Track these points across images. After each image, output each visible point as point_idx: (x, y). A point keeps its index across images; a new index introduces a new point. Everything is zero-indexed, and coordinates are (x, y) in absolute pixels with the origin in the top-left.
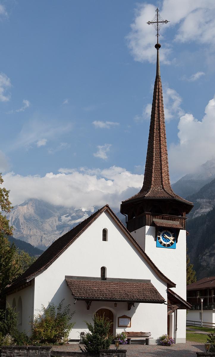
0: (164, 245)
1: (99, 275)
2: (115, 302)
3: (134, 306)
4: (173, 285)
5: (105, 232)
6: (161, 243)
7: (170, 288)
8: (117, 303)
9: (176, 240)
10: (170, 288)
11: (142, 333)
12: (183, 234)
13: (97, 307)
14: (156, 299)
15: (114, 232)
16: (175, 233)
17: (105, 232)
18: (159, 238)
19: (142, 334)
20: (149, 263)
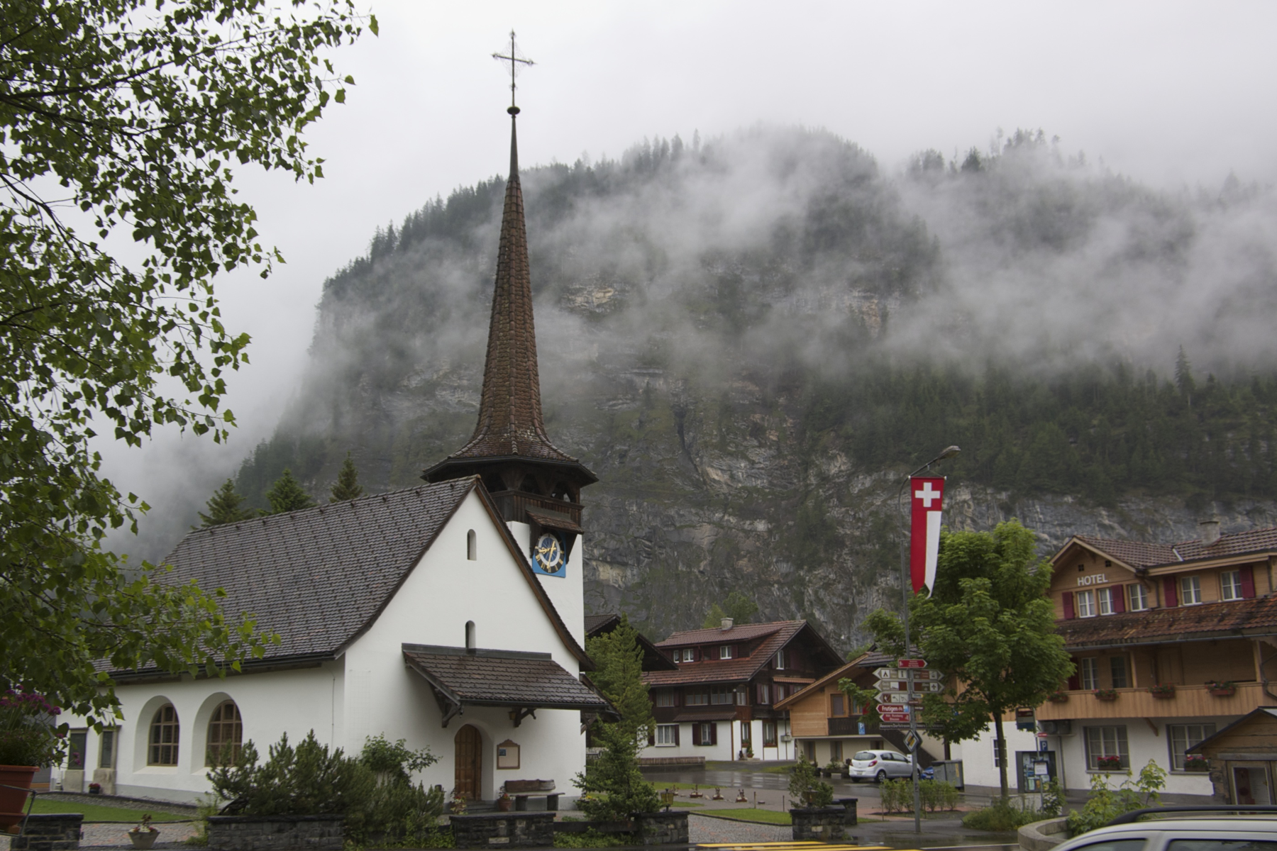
5: (471, 535)
17: (471, 535)
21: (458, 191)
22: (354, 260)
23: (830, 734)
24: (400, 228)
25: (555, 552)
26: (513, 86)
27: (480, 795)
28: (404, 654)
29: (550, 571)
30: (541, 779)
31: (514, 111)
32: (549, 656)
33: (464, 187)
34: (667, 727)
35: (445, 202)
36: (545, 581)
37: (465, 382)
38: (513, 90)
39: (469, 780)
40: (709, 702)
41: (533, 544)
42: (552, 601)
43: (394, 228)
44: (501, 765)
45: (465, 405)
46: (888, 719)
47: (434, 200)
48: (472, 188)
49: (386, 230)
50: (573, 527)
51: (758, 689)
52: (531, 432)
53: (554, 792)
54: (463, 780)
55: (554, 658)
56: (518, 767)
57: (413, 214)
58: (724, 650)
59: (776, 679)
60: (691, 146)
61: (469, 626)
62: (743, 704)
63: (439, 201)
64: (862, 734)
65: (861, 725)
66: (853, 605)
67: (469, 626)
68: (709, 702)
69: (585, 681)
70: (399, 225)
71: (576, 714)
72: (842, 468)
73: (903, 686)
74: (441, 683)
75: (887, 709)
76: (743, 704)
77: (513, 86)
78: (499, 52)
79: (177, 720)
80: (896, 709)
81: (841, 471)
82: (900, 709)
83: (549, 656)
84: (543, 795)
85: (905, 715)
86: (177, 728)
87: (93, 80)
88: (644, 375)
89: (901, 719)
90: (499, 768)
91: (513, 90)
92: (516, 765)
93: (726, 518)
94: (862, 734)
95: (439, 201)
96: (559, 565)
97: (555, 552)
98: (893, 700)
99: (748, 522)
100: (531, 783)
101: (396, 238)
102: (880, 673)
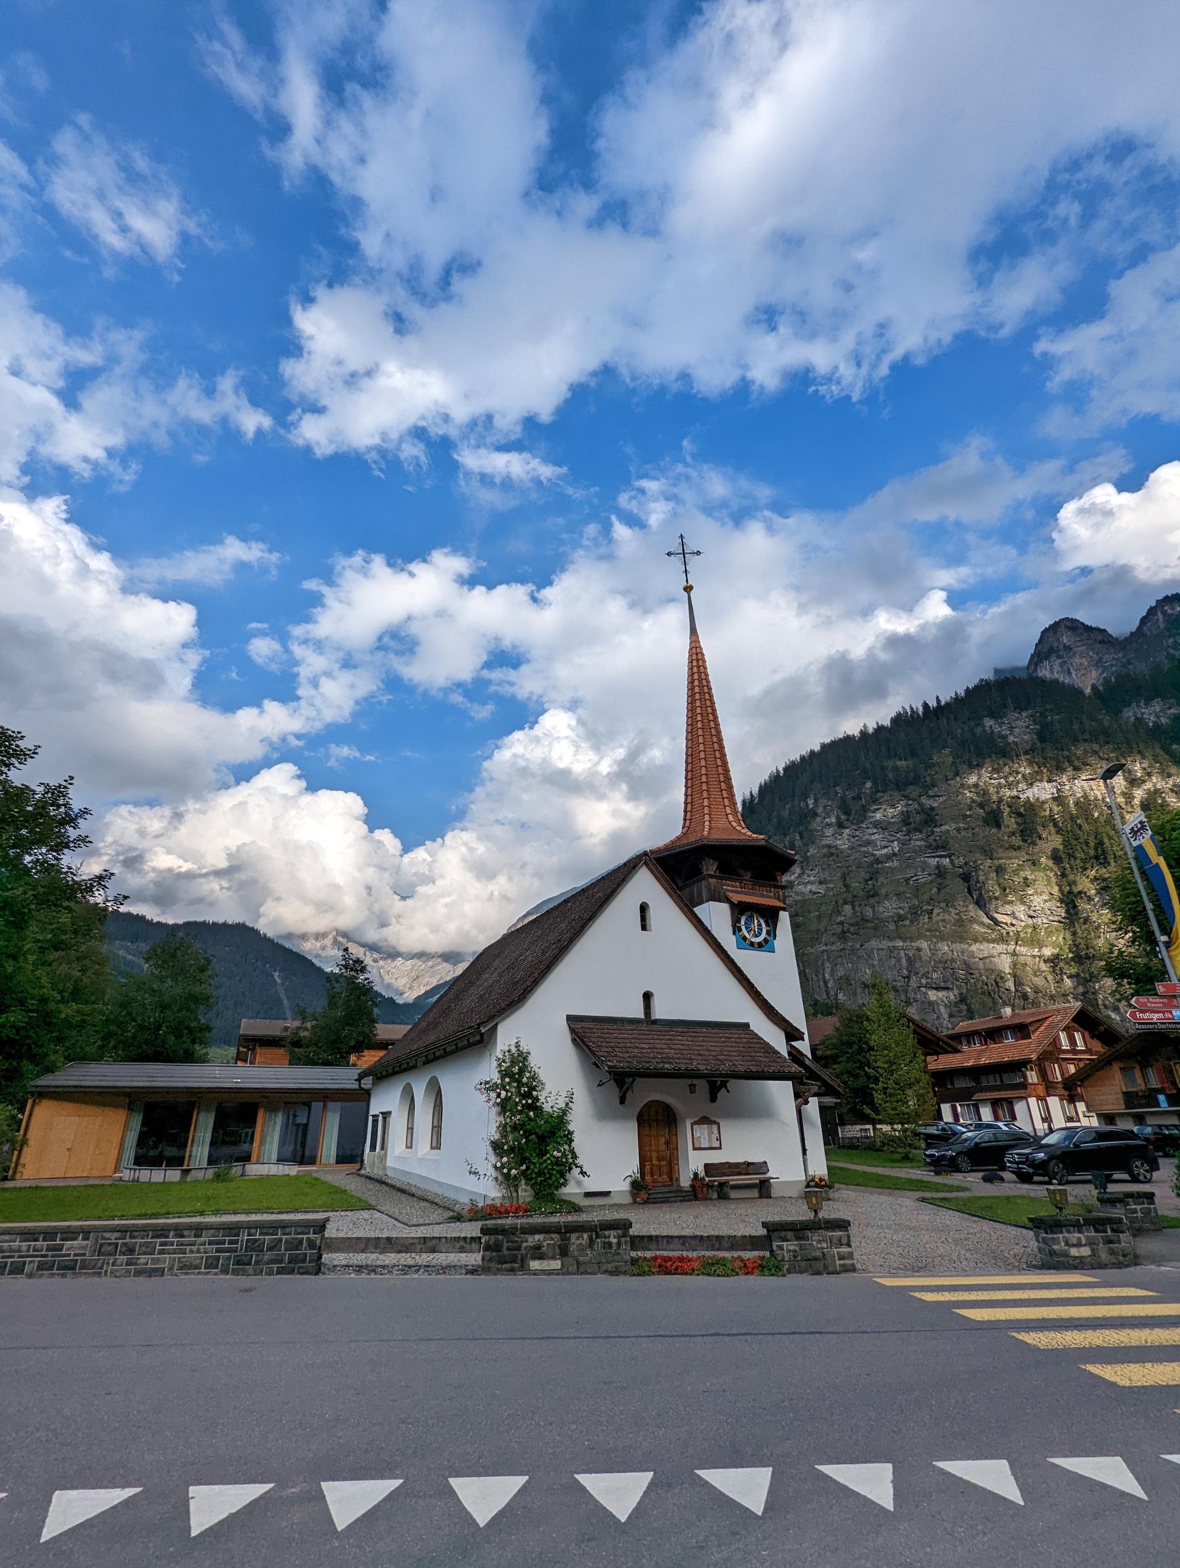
0: (752, 944)
1: (640, 1014)
2: (689, 1081)
3: (728, 1091)
4: (796, 1034)
5: (644, 908)
6: (745, 938)
7: (793, 1043)
8: (695, 1081)
9: (772, 933)
10: (793, 1043)
11: (749, 1164)
12: (784, 916)
13: (646, 1093)
14: (754, 1069)
15: (664, 908)
16: (771, 916)
17: (644, 908)
18: (740, 930)
19: (747, 1168)
20: (403, 1191)
25: (760, 925)
27: (678, 1180)
28: (572, 1031)
29: (756, 946)
32: (747, 1025)
34: (968, 1105)
37: (812, 878)
40: (1002, 1080)
42: (742, 969)
44: (697, 1145)
45: (815, 893)
51: (1048, 1069)
53: (769, 1175)
56: (720, 1148)
60: (935, 704)
61: (647, 996)
62: (1036, 1081)
63: (778, 771)
67: (647, 996)
68: (1002, 1080)
70: (756, 791)
78: (672, 550)
84: (755, 1179)
87: (315, 588)
88: (934, 857)
90: (695, 1149)
93: (1018, 948)
95: (778, 771)
96: (766, 941)
97: (760, 925)
99: (1037, 950)
100: (737, 1165)
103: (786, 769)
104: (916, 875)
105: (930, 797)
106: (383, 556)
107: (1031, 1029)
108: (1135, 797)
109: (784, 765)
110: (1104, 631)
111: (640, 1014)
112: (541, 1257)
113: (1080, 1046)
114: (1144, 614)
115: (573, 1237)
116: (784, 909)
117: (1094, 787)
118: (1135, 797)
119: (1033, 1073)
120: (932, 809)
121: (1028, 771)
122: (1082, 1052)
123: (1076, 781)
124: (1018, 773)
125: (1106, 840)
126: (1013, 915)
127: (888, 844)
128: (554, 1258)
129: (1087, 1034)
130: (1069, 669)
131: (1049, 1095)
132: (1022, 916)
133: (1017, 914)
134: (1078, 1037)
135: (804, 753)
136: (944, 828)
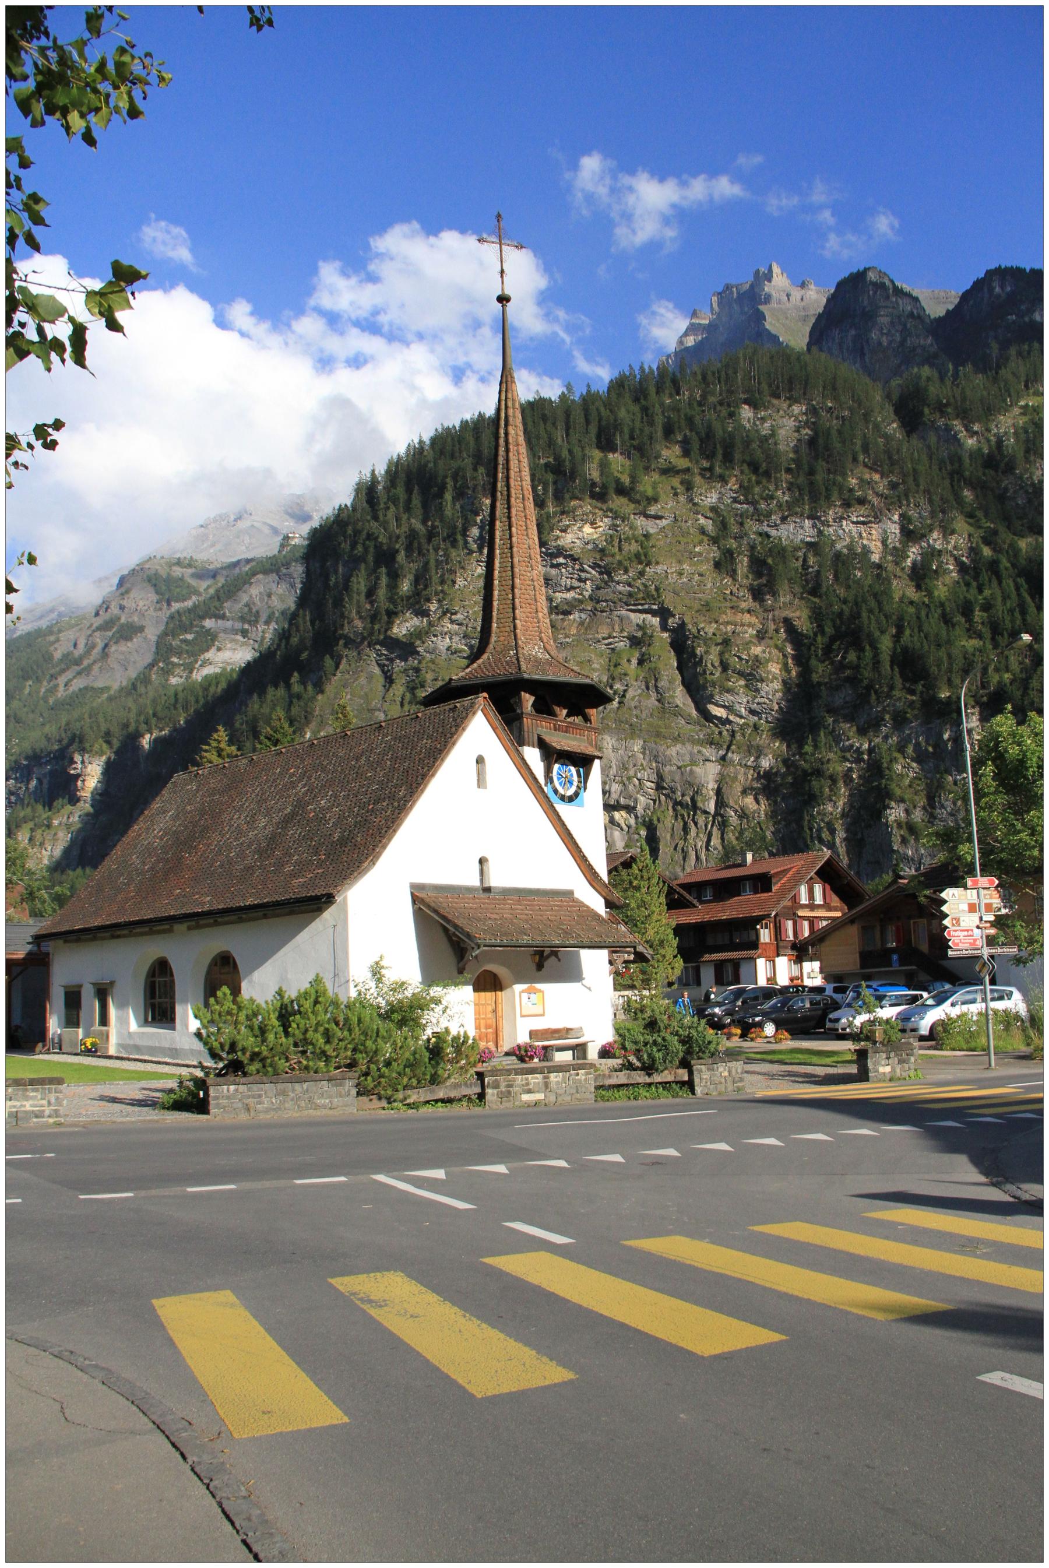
5: (480, 760)
16: (583, 762)
17: (480, 760)
21: (440, 430)
22: (337, 507)
23: (862, 967)
24: (383, 472)
26: (502, 272)
30: (569, 1026)
31: (503, 299)
32: (571, 893)
33: (446, 426)
35: (428, 442)
36: (564, 810)
38: (502, 277)
39: (490, 1030)
41: (548, 771)
43: (377, 473)
44: (524, 1013)
46: (957, 944)
47: (416, 441)
48: (454, 427)
49: (369, 475)
50: (590, 751)
52: (540, 648)
54: (483, 1030)
55: (577, 895)
56: (543, 1015)
57: (395, 457)
58: (744, 886)
59: (800, 913)
62: (767, 940)
64: (896, 967)
65: (895, 957)
66: (862, 839)
69: (613, 920)
70: (381, 470)
71: (603, 954)
72: (847, 699)
73: (972, 908)
74: (456, 926)
75: (956, 934)
76: (767, 940)
77: (502, 272)
79: (172, 975)
80: (965, 933)
81: (846, 703)
82: (970, 933)
83: (571, 893)
85: (975, 940)
86: (173, 982)
89: (971, 944)
90: (522, 1016)
91: (502, 277)
92: (541, 1012)
93: (730, 755)
94: (896, 967)
95: (421, 442)
96: (577, 794)
98: (962, 924)
101: (379, 482)
102: (948, 895)
103: (434, 440)
104: (610, 637)
105: (647, 517)
106: (239, 299)
107: (774, 880)
108: (908, 557)
109: (432, 433)
110: (916, 300)
111: (474, 881)
112: (529, 1091)
113: (819, 900)
114: (969, 287)
115: (552, 1075)
116: (600, 758)
117: (864, 535)
118: (908, 557)
119: (767, 931)
120: (647, 536)
121: (786, 498)
122: (819, 906)
123: (844, 523)
124: (772, 497)
125: (864, 614)
126: (729, 708)
127: (576, 584)
128: (538, 1092)
129: (828, 887)
130: (862, 348)
131: (778, 955)
132: (743, 710)
133: (737, 707)
134: (818, 889)
135: (468, 417)
136: (659, 569)
